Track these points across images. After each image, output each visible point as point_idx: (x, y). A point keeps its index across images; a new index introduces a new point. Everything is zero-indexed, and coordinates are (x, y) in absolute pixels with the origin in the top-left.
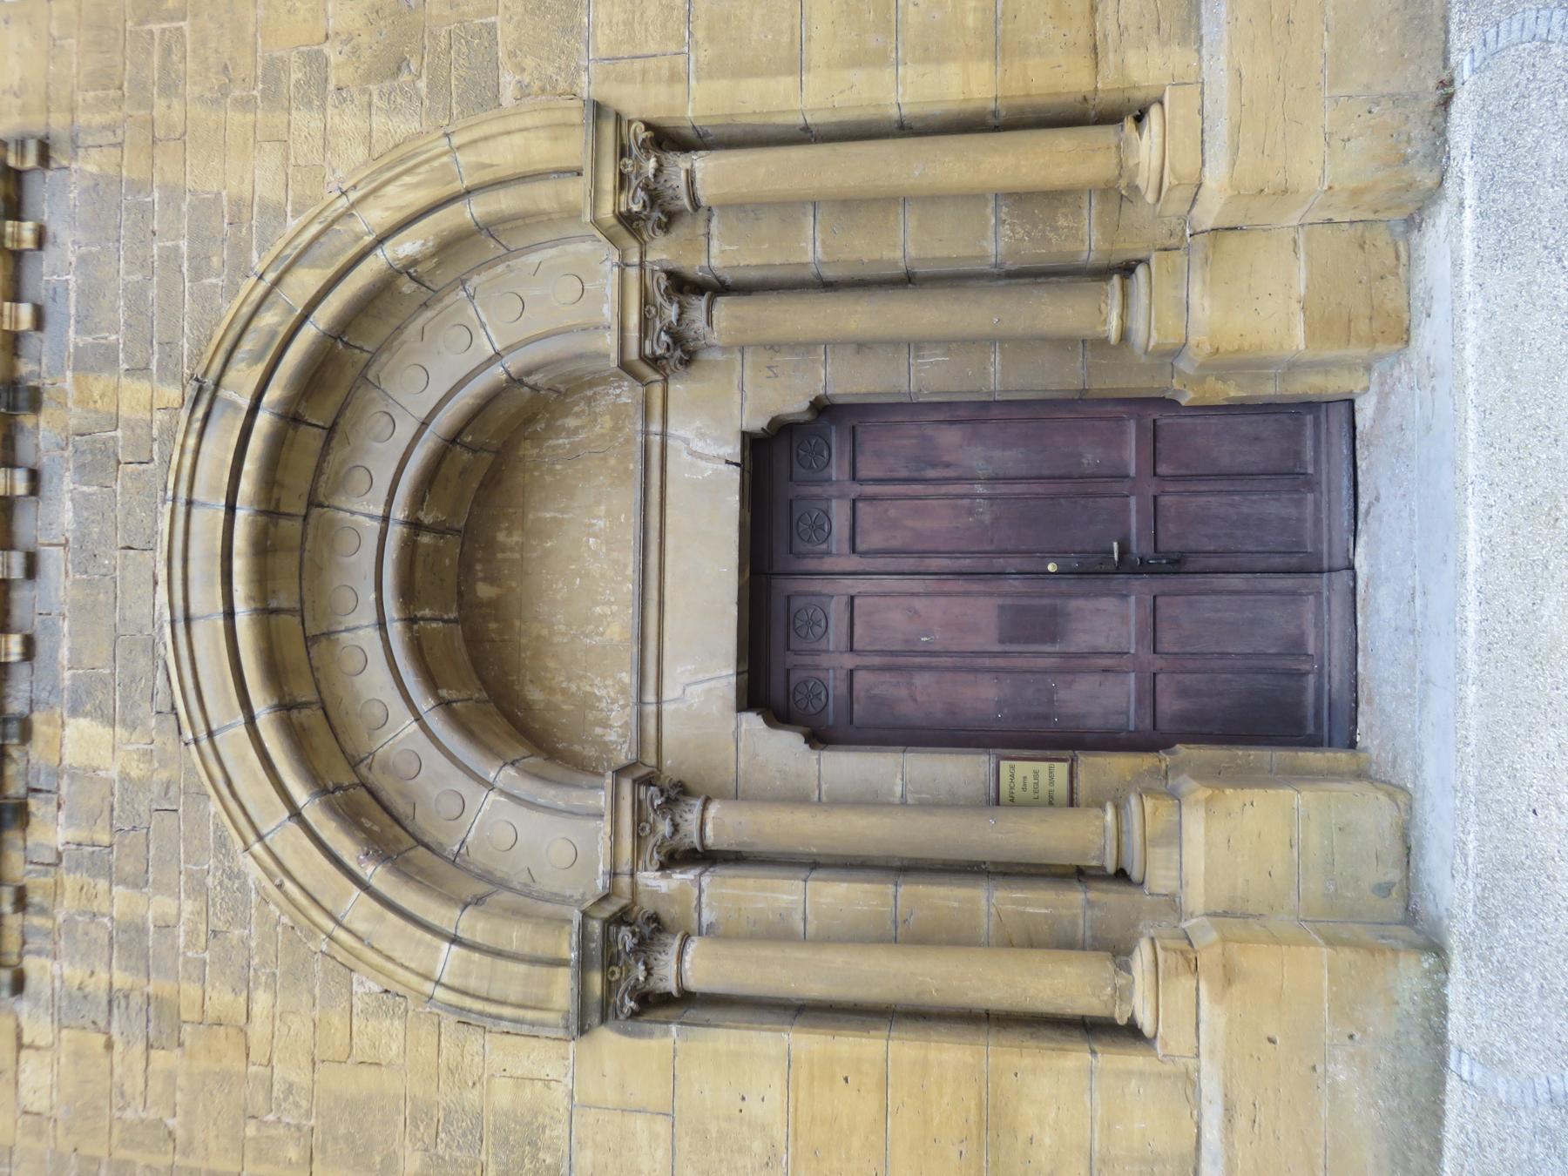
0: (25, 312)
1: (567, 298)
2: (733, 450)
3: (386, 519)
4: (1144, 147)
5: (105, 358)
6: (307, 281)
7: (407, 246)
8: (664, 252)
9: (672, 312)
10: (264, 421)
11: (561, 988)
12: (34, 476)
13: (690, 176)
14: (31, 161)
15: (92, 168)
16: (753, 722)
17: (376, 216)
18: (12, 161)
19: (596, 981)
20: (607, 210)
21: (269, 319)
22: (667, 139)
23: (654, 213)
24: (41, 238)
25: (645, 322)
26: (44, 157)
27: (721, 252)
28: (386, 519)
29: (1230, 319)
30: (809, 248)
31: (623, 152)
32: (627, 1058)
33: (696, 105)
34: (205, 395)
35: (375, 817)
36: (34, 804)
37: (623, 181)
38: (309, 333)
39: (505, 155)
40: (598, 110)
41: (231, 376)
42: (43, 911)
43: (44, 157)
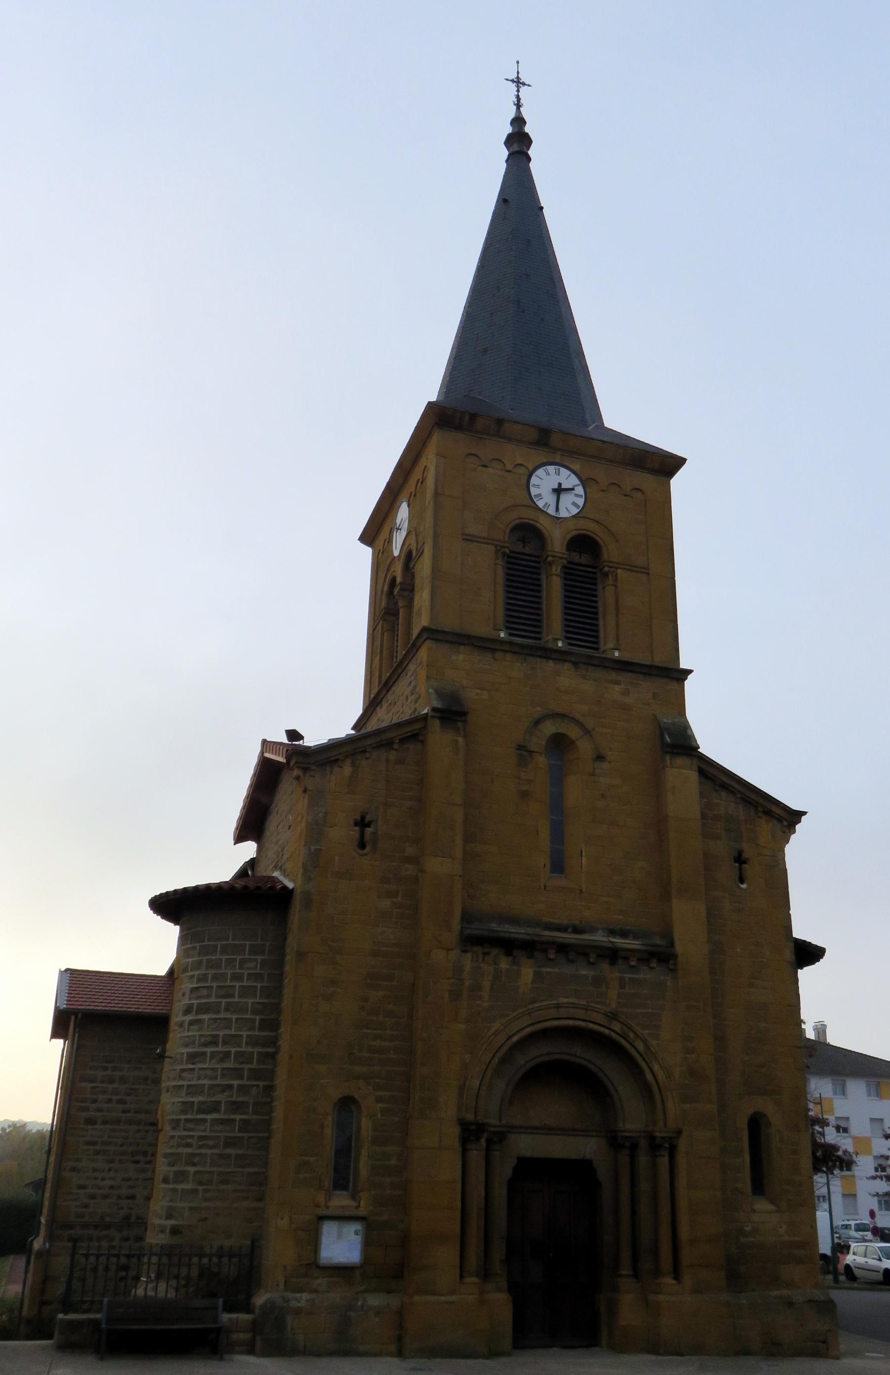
0: (633, 963)
1: (632, 1120)
2: (588, 1157)
3: (576, 1056)
4: (669, 1280)
5: (622, 986)
6: (641, 1046)
7: (649, 1076)
8: (643, 1143)
9: (627, 1144)
10: (607, 1032)
11: (470, 1117)
12: (593, 963)
13: (664, 1156)
14: (671, 967)
15: (669, 983)
16: (514, 1162)
17: (656, 1067)
18: (671, 962)
19: (473, 1127)
20: (657, 1134)
21: (632, 1035)
22: (673, 1150)
23: (654, 1145)
24: (652, 968)
25: (626, 1137)
26: (671, 970)
27: (643, 1160)
28: (576, 1056)
29: (629, 1310)
30: (644, 1186)
31: (670, 1138)
32: (453, 1132)
33: (682, 1161)
34: (613, 1016)
35: (507, 1058)
36: (511, 958)
37: (663, 1138)
38: (628, 1046)
39: (670, 1105)
40: (679, 1132)
41: (618, 1024)
42: (483, 960)
43: (671, 970)
